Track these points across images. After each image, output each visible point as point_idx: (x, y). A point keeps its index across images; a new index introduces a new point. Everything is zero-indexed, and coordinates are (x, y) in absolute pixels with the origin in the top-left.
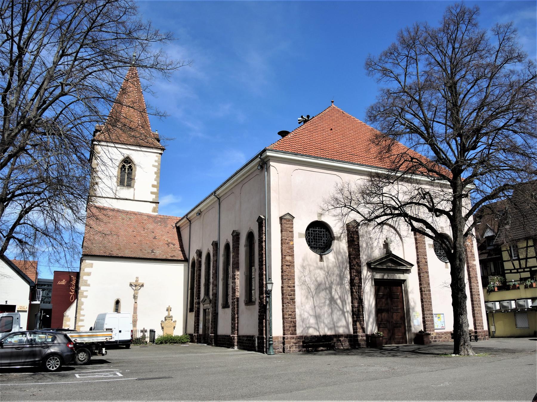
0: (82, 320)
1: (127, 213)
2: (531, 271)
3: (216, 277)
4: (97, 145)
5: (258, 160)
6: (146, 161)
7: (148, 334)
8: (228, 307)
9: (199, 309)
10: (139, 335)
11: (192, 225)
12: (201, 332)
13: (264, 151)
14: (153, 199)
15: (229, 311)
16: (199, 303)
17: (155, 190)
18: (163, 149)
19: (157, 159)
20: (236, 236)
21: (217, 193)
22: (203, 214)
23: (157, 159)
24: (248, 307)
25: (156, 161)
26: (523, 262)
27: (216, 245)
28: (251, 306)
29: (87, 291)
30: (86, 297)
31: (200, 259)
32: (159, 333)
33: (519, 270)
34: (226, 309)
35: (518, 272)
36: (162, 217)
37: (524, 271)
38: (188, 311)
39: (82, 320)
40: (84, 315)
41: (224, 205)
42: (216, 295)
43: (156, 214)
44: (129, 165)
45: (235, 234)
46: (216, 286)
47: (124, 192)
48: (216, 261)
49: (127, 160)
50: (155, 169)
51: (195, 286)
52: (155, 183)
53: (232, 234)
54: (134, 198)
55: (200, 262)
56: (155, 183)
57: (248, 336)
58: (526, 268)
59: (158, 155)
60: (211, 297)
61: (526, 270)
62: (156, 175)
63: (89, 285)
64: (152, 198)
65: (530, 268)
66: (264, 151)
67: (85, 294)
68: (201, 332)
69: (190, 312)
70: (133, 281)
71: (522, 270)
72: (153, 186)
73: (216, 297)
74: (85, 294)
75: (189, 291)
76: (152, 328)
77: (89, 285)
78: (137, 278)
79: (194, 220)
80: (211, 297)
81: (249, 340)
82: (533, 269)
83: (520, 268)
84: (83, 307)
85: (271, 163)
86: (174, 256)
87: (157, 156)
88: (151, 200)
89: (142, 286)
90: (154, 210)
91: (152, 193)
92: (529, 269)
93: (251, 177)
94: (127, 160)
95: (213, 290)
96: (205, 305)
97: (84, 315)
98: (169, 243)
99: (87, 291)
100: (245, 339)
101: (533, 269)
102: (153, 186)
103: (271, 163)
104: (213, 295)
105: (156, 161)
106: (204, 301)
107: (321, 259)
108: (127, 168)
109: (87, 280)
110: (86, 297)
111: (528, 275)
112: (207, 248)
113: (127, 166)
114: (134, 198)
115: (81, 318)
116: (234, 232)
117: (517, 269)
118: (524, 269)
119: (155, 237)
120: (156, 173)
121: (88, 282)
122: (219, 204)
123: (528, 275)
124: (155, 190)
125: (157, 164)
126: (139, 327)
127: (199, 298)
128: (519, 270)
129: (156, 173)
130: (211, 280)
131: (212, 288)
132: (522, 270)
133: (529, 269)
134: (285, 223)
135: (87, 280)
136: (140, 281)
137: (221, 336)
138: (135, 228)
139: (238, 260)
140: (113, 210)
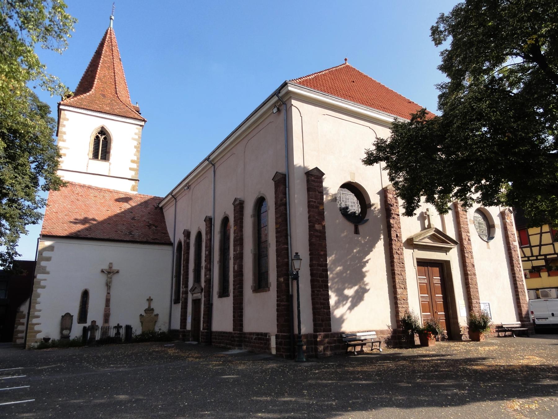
0: (38, 317)
1: (100, 190)
2: (546, 260)
3: (210, 259)
4: (64, 110)
5: (275, 99)
6: (125, 136)
7: (122, 331)
8: (228, 295)
9: (186, 299)
10: (112, 333)
11: (178, 203)
12: (189, 327)
13: (285, 84)
14: (132, 176)
15: (229, 302)
16: (186, 293)
17: (135, 166)
18: (144, 121)
19: (137, 131)
20: (239, 206)
21: (212, 158)
22: (192, 187)
23: (137, 131)
24: (258, 294)
25: (136, 134)
26: (536, 251)
27: (209, 221)
28: (262, 294)
29: (45, 280)
30: (44, 287)
31: (188, 241)
32: (137, 330)
33: (531, 258)
34: (225, 299)
35: (529, 260)
36: (142, 196)
37: (537, 259)
38: (173, 303)
39: (38, 317)
40: (40, 311)
41: (220, 171)
42: (209, 282)
43: (135, 193)
44: (103, 137)
45: (237, 202)
46: (209, 270)
47: (99, 166)
48: (210, 241)
49: (103, 131)
50: (135, 143)
51: (182, 272)
52: (135, 158)
53: (234, 204)
54: (109, 173)
55: (188, 245)
56: (135, 158)
57: (258, 334)
58: (540, 255)
59: (139, 127)
60: (203, 284)
61: (539, 257)
62: (136, 150)
63: (48, 273)
64: (131, 174)
65: (545, 255)
66: (285, 84)
67: (42, 283)
68: (189, 327)
69: (175, 303)
70: (106, 267)
71: (535, 258)
72: (133, 161)
73: (210, 284)
74: (42, 283)
75: (174, 279)
76: (129, 324)
77: (48, 273)
78: (111, 264)
79: (180, 196)
80: (203, 284)
81: (260, 339)
82: (548, 257)
83: (532, 256)
84: (38, 300)
85: (294, 102)
86: (156, 239)
87: (137, 128)
88: (130, 178)
89: (118, 272)
90: (133, 189)
91: (131, 169)
92: (543, 257)
93: (261, 127)
94: (103, 131)
95: (205, 275)
96: (195, 295)
97: (40, 311)
98: (151, 225)
99: (45, 280)
100: (254, 337)
101: (548, 257)
102: (133, 161)
103: (294, 102)
104: (205, 282)
105: (136, 134)
106: (193, 290)
107: (357, 232)
108: (102, 147)
109: (45, 267)
110: (44, 287)
111: (542, 263)
112: (197, 225)
113: (102, 138)
114: (109, 173)
115: (37, 313)
116: (236, 200)
117: (528, 257)
118: (537, 256)
119: (134, 217)
120: (135, 147)
121: (48, 269)
122: (214, 172)
123: (542, 263)
124: (135, 166)
125: (137, 137)
126: (113, 323)
127: (187, 286)
128: (531, 258)
129: (135, 147)
130: (203, 264)
131: (205, 273)
132: (535, 258)
133: (543, 257)
134: (314, 181)
135: (45, 267)
136: (115, 268)
137: (216, 332)
138: (109, 207)
139: (242, 235)
140: (83, 186)
